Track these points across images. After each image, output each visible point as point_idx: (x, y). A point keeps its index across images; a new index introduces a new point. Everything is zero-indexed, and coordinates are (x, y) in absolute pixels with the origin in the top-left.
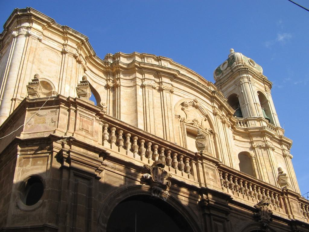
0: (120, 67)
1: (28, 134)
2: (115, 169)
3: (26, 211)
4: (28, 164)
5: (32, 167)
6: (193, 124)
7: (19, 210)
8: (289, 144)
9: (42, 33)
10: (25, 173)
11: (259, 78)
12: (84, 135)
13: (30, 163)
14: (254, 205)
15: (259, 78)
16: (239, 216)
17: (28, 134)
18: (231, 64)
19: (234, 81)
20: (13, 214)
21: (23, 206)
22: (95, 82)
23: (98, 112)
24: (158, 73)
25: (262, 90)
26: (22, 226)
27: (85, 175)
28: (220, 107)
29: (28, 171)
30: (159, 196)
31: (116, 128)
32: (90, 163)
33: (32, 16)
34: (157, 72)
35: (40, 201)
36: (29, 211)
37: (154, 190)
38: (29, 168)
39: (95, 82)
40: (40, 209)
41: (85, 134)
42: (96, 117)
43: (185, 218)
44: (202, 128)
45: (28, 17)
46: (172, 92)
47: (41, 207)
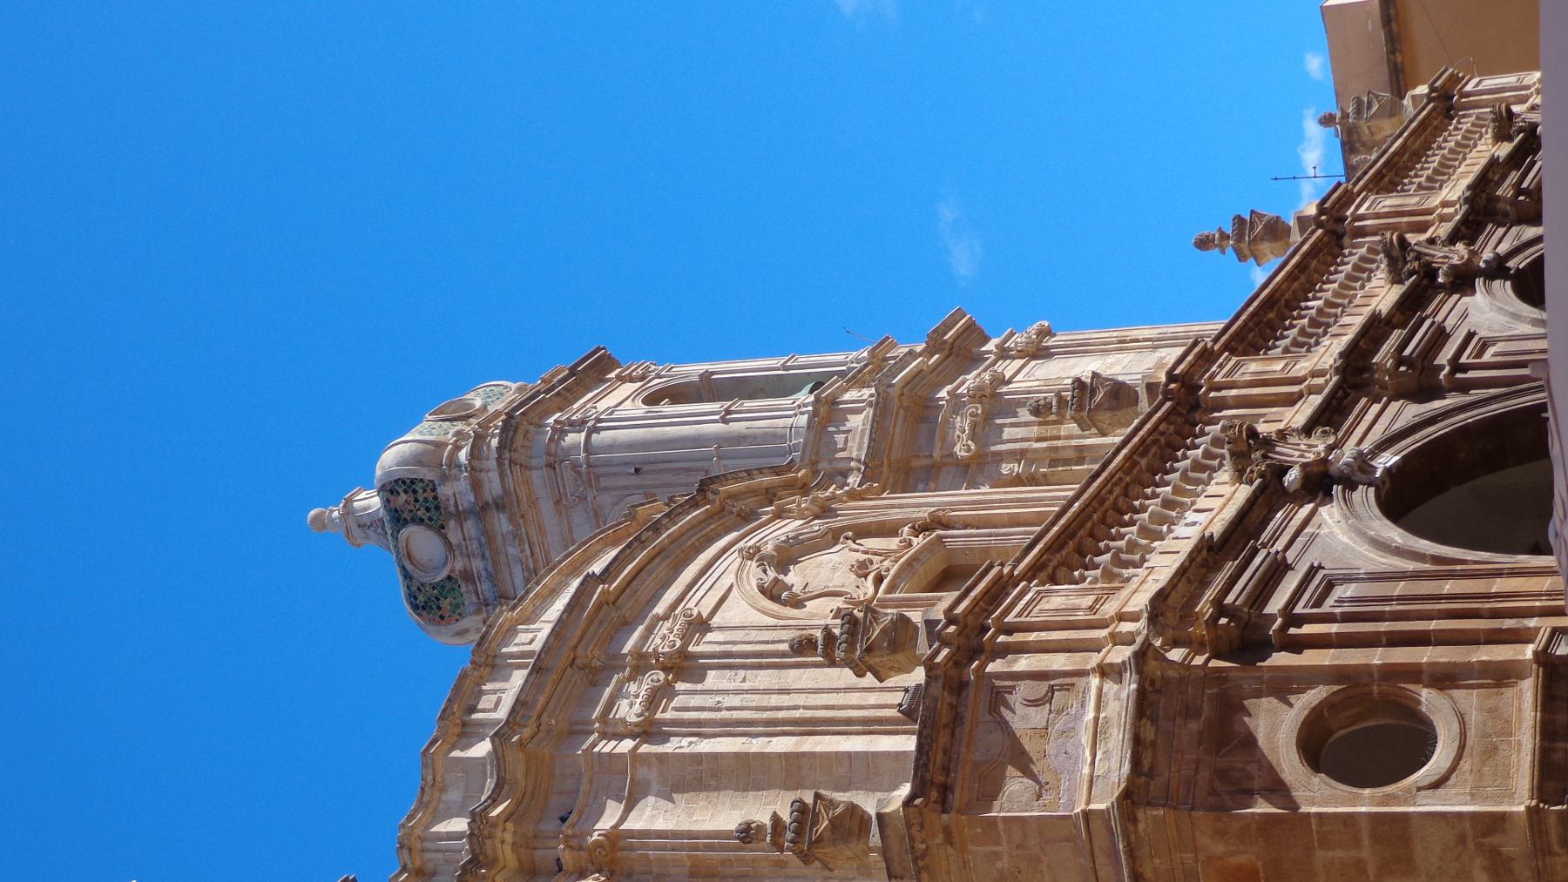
18: (437, 508)
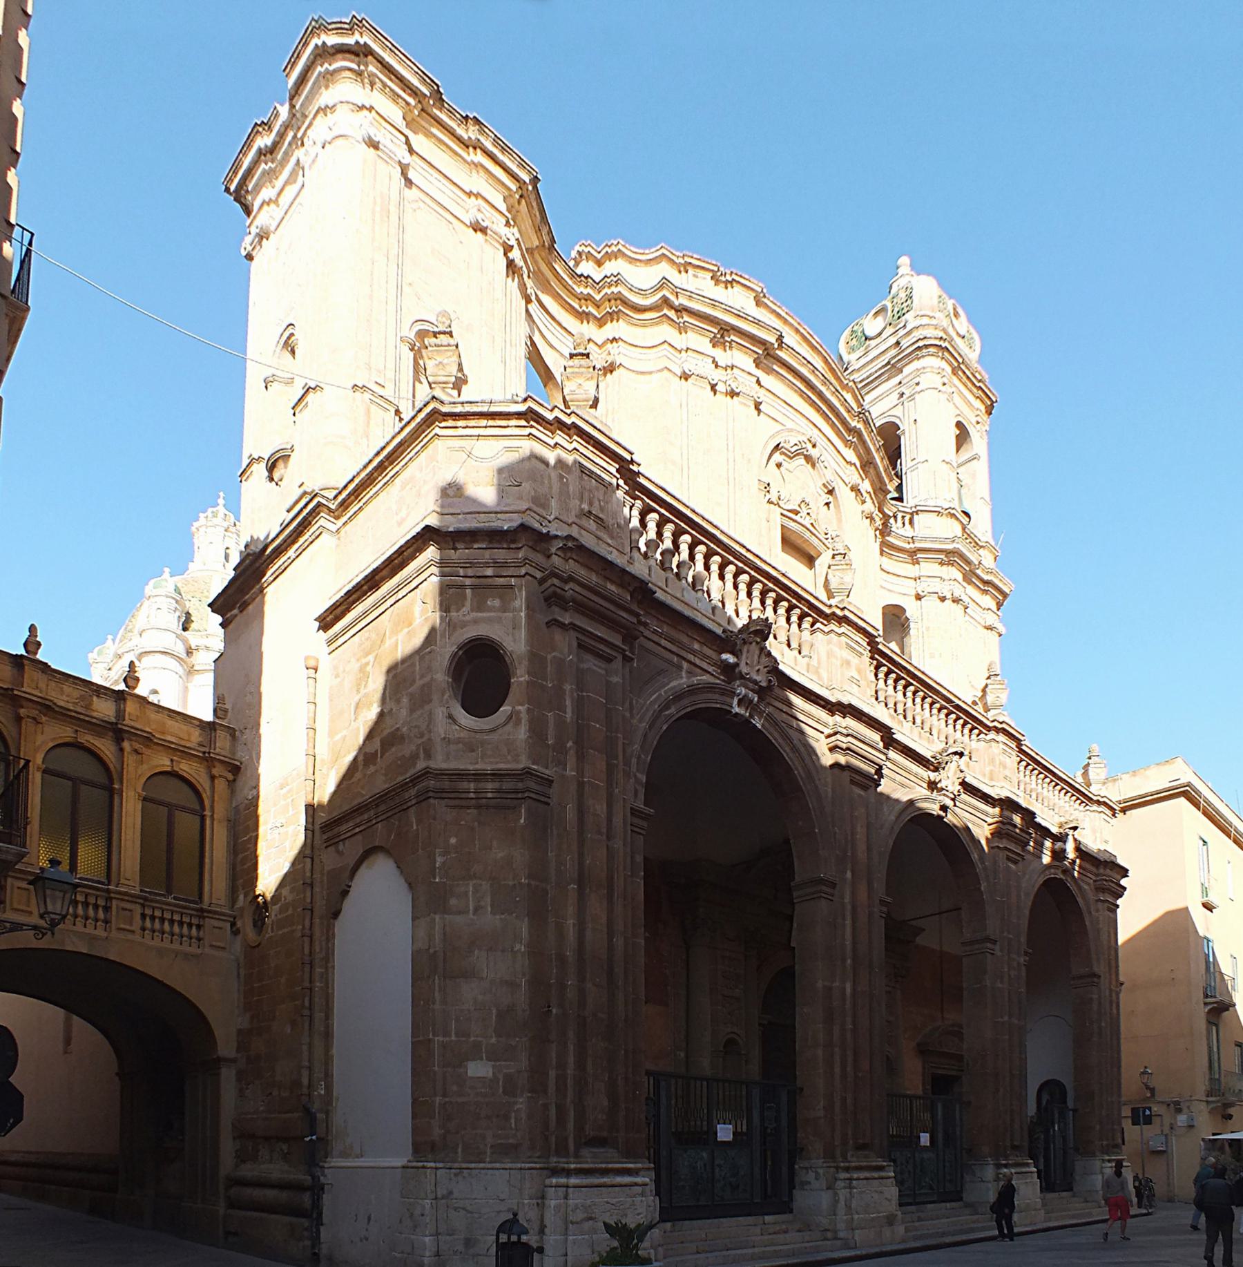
0: (621, 300)
1: (452, 514)
2: (660, 635)
3: (475, 731)
4: (463, 606)
5: (474, 614)
6: (797, 513)
7: (457, 727)
8: (1005, 595)
9: (407, 137)
10: (459, 631)
11: (968, 378)
12: (594, 530)
13: (468, 603)
14: (932, 754)
15: (968, 378)
16: (898, 778)
17: (452, 514)
19: (896, 380)
20: (442, 736)
21: (465, 719)
22: (552, 346)
23: (622, 464)
24: (725, 332)
25: (969, 419)
26: (62, 704)
27: (602, 647)
28: (865, 466)
29: (464, 625)
30: (748, 714)
31: (661, 515)
32: (606, 611)
33: (370, 57)
34: (721, 328)
35: (506, 709)
36: (482, 731)
37: (741, 697)
38: (467, 618)
39: (552, 346)
40: (509, 727)
41: (597, 530)
42: (618, 479)
43: (796, 772)
44: (816, 526)
45: (357, 59)
46: (757, 406)
47: (511, 724)
